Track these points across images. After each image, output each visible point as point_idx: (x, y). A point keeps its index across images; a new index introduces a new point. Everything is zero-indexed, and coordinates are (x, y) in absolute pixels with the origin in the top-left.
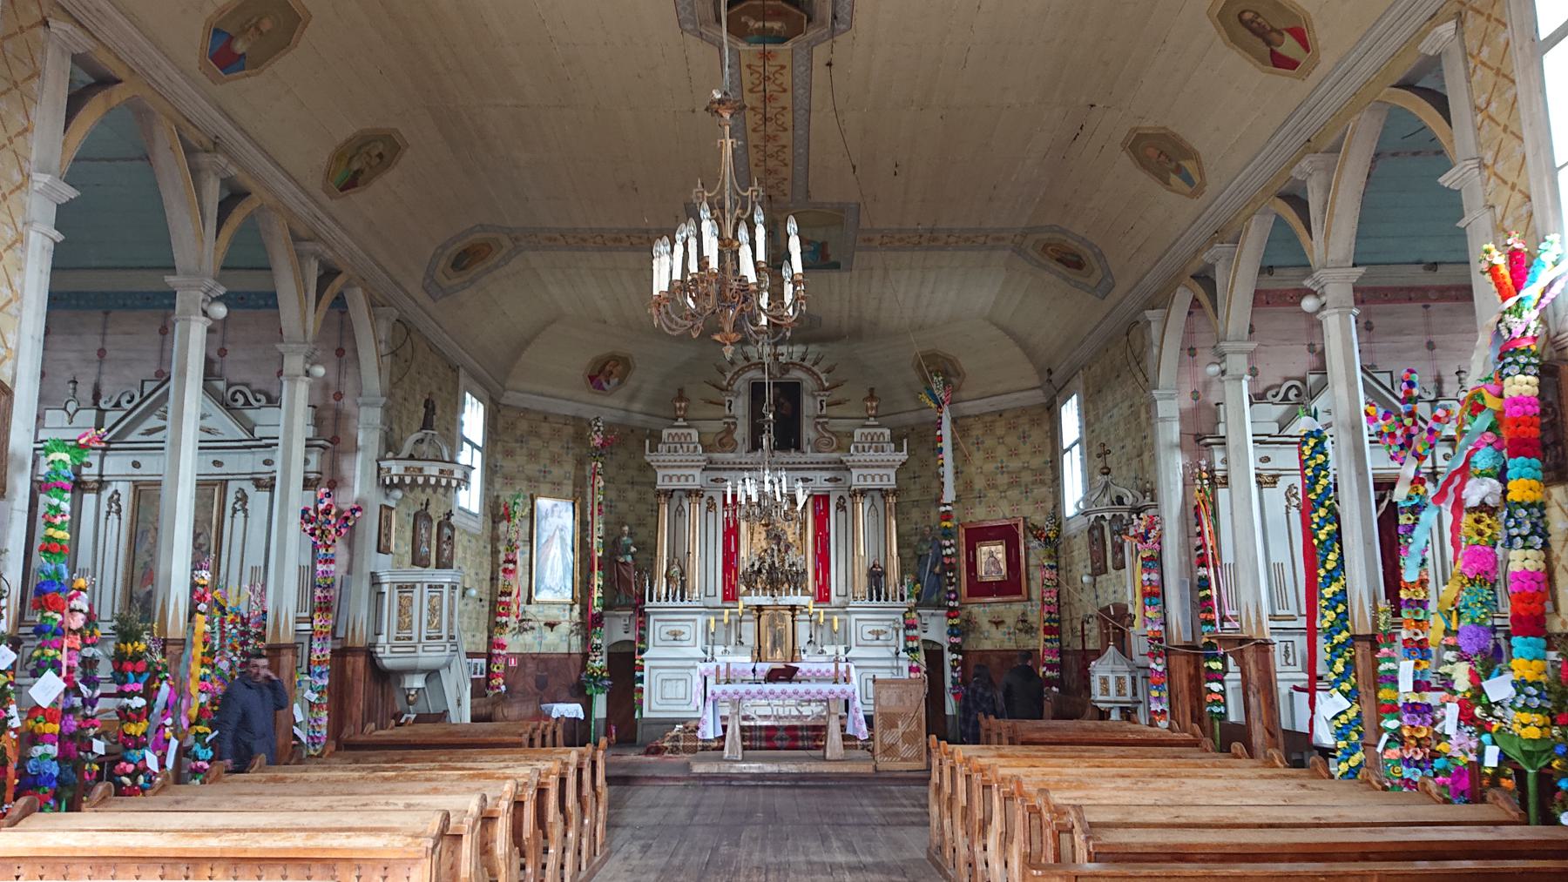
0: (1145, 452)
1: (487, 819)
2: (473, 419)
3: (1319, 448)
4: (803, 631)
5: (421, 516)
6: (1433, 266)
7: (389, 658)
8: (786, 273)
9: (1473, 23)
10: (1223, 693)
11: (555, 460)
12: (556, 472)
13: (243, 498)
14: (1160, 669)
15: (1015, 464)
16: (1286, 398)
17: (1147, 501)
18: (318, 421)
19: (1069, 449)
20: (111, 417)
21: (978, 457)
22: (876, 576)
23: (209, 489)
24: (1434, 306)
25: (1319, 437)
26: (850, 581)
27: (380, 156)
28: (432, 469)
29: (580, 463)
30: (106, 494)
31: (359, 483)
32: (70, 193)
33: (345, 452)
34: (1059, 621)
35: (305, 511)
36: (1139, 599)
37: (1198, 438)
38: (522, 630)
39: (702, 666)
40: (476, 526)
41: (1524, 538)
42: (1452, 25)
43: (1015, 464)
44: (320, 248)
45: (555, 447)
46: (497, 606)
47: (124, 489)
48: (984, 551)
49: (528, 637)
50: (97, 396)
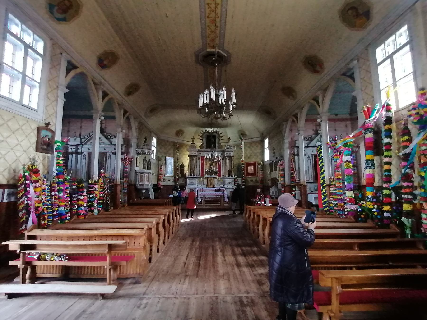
0: (281, 149)
1: (158, 224)
2: (154, 141)
3: (320, 148)
4: (216, 182)
5: (144, 160)
7: (138, 186)
8: (230, 103)
9: (362, 61)
10: (295, 194)
11: (169, 150)
13: (110, 156)
15: (255, 151)
16: (308, 140)
17: (282, 159)
18: (124, 141)
20: (83, 140)
22: (230, 172)
23: (102, 155)
25: (321, 146)
28: (146, 151)
29: (174, 150)
30: (83, 155)
31: (132, 151)
32: (67, 91)
33: (129, 147)
35: (122, 159)
37: (292, 147)
38: (164, 181)
39: (197, 188)
40: (155, 162)
41: (370, 167)
42: (356, 61)
43: (255, 151)
46: (159, 176)
47: (87, 154)
48: (249, 167)
49: (165, 182)
50: (80, 136)
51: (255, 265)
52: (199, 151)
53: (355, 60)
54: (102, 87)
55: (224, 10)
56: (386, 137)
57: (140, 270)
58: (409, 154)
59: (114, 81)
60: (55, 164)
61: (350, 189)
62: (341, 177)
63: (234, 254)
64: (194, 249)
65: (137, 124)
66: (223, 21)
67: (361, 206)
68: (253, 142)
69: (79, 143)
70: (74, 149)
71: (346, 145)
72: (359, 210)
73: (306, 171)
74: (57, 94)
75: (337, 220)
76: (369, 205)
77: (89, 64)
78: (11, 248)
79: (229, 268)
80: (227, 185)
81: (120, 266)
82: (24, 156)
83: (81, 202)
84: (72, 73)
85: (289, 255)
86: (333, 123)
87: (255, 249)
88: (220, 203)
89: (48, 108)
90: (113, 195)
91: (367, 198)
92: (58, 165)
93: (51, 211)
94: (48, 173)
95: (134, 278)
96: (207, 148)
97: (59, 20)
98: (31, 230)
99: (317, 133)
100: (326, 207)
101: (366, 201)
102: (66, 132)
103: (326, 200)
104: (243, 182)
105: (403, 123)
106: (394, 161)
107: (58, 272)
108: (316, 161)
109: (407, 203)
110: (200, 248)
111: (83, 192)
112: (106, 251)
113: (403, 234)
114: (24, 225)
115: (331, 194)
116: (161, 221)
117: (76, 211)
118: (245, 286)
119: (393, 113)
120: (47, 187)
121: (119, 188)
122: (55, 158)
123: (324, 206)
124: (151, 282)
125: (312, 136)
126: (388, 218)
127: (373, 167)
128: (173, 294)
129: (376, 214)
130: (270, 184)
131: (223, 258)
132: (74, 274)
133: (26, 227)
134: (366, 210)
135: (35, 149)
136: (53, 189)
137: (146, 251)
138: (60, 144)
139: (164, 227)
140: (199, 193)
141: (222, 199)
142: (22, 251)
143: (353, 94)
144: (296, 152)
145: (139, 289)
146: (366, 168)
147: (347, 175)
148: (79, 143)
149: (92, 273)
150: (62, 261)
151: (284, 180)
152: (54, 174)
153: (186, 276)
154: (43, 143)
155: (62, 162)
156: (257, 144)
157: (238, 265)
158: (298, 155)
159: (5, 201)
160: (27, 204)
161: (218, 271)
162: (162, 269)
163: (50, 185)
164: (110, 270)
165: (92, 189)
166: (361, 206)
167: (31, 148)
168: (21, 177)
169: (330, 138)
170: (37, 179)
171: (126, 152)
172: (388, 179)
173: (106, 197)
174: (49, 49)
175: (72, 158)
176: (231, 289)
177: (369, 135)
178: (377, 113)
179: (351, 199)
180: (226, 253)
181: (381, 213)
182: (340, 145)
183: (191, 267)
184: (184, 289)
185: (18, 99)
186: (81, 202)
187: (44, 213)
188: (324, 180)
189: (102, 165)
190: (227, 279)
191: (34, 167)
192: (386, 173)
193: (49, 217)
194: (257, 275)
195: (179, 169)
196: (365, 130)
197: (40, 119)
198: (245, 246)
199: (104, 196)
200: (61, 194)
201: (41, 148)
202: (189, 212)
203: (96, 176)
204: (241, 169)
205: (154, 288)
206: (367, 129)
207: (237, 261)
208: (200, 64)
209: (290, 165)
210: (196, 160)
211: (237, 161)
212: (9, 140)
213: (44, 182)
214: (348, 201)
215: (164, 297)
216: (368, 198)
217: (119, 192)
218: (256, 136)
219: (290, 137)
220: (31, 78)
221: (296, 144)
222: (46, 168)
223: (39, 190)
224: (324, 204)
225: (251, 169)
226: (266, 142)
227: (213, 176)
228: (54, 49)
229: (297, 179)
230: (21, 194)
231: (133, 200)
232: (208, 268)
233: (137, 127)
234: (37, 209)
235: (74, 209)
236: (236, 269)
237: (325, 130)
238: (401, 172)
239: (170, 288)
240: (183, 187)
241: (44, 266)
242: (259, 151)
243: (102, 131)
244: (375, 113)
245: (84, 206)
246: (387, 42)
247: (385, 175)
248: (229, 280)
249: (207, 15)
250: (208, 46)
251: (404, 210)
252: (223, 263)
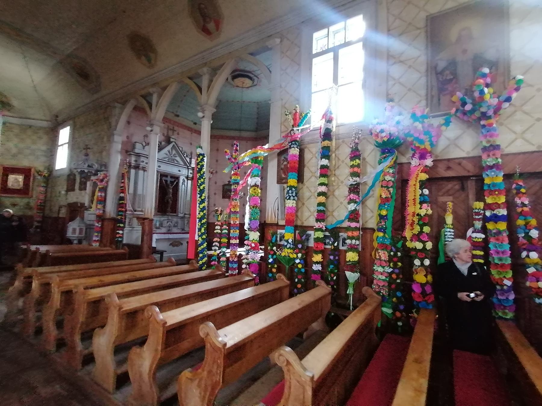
0: (104, 151)
3: (202, 160)
10: (123, 234)
14: (100, 226)
15: (34, 147)
17: (103, 168)
19: (62, 145)
24: (194, 134)
34: (44, 206)
37: (127, 152)
75: (144, 265)
151: (104, 207)
226: (65, 134)
242: (44, 148)
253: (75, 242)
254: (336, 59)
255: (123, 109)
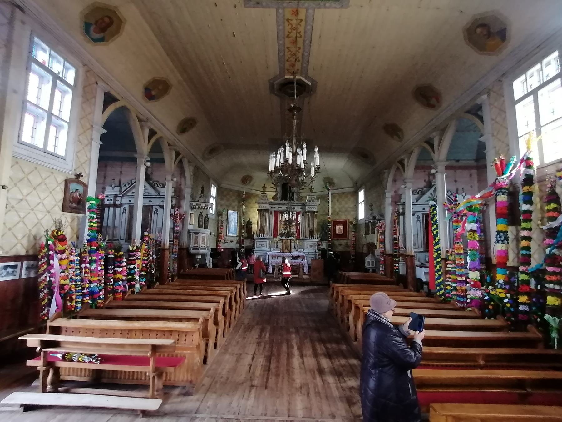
0: (381, 205)
2: (214, 190)
4: (293, 245)
5: (200, 215)
6: (458, 161)
7: (192, 250)
10: (398, 266)
11: (233, 201)
12: (234, 204)
13: (156, 210)
15: (347, 206)
16: (418, 193)
17: (382, 218)
18: (175, 192)
20: (123, 189)
21: (337, 204)
22: (311, 233)
23: (147, 209)
25: (435, 206)
26: (305, 233)
27: (191, 124)
28: (203, 204)
29: (239, 202)
30: (122, 208)
31: (185, 204)
32: (105, 131)
35: (171, 214)
36: (378, 243)
37: (396, 203)
38: (224, 242)
39: (268, 253)
40: (214, 217)
41: (502, 241)
43: (347, 206)
44: (176, 148)
45: (233, 198)
46: (218, 236)
48: (338, 227)
49: (226, 244)
51: (344, 374)
52: (271, 204)
53: (485, 94)
54: (149, 124)
55: (309, 27)
56: (526, 202)
57: (191, 375)
58: (557, 229)
59: (163, 116)
60: (87, 228)
61: (474, 269)
62: (462, 251)
63: (316, 355)
64: (263, 344)
65: (192, 168)
66: (307, 42)
67: (489, 294)
68: (343, 193)
69: (118, 193)
70: (111, 200)
71: (470, 208)
72: (486, 298)
73: (414, 236)
74: (92, 135)
76: (500, 293)
77: (132, 96)
78: (29, 345)
79: (309, 377)
80: (308, 250)
81: (167, 374)
82: (48, 217)
83: (118, 276)
84: (111, 108)
85: (388, 381)
86: (452, 172)
87: (344, 347)
88: (298, 274)
89: (79, 155)
90: (160, 262)
91: (497, 284)
92: (91, 228)
93: (81, 288)
94: (78, 238)
95: (184, 387)
96: (282, 200)
97: (95, 41)
98: (55, 318)
99: (430, 185)
100: (441, 289)
101: (496, 287)
102: (101, 187)
103: (441, 280)
104: (329, 246)
105: (549, 185)
106: (535, 235)
107: (87, 375)
108: (428, 221)
109: (553, 296)
110: (271, 342)
111: (121, 262)
112: (149, 354)
113: (547, 341)
114: (46, 309)
115: (447, 272)
116: (221, 306)
117: (112, 287)
118: (330, 406)
119: (535, 170)
120: (75, 258)
121: (167, 253)
122: (88, 219)
123: (438, 288)
124: (206, 393)
125: (423, 189)
126: (524, 312)
127: (506, 242)
128: (234, 414)
129: (508, 305)
130: (365, 250)
131: (301, 360)
132: (109, 378)
133: (49, 310)
134: (495, 300)
135: (61, 208)
136: (84, 259)
137: (200, 352)
138: (94, 202)
139: (224, 314)
140: (271, 260)
141: (301, 270)
142: (43, 350)
143: (482, 139)
144: (401, 210)
145: (190, 403)
146: (498, 241)
147: (470, 250)
148: (118, 193)
149: (131, 378)
150: (93, 363)
151: (385, 246)
152: (86, 241)
153: (252, 386)
154: (71, 200)
155: (95, 225)
156: (349, 196)
157: (321, 372)
158: (404, 214)
159: (23, 276)
160: (50, 281)
161: (293, 380)
162: (220, 374)
163: (80, 255)
164: (154, 377)
165: (133, 258)
166: (489, 294)
167: (57, 206)
168: (42, 247)
169: (448, 192)
170: (63, 248)
171: (176, 206)
172: (526, 260)
173: (151, 265)
174: (81, 80)
175: (109, 212)
176: (311, 410)
177: (502, 198)
178: (514, 168)
179: (475, 283)
180: (304, 352)
181: (515, 304)
182: (462, 208)
183: (258, 372)
184: (248, 407)
185: (41, 146)
186: (118, 276)
187: (71, 292)
188: (439, 252)
189: (145, 226)
190: (306, 393)
191: (59, 233)
192: (524, 252)
193: (78, 297)
194: (346, 390)
195: (245, 227)
196: (496, 190)
197: (70, 171)
198: (330, 341)
199: (148, 263)
200: (94, 266)
201: (70, 207)
202: (257, 287)
203: (138, 241)
204: (327, 228)
205: (210, 403)
206: (499, 189)
207: (319, 364)
208: (276, 95)
209: (392, 227)
210: (267, 215)
211: (322, 217)
212: (28, 198)
213: (72, 252)
214: (472, 285)
215: (222, 418)
216: (499, 283)
217: (167, 259)
218: (348, 187)
219: (394, 190)
220: (58, 117)
221: (401, 199)
222: (76, 231)
223: (65, 262)
224: (439, 286)
225: (340, 228)
227: (290, 238)
228: (87, 76)
229: (401, 246)
230: (42, 269)
231: (185, 271)
232: (281, 375)
233: (192, 174)
234: (62, 287)
235: (110, 285)
236: (318, 378)
237: (442, 182)
238: (545, 251)
239: (231, 403)
240: (249, 251)
241: (70, 368)
242: (352, 206)
243: (148, 178)
244: (510, 169)
245: (123, 281)
246: (529, 73)
247: (522, 254)
248: (308, 395)
249: (287, 33)
250: (286, 71)
251: (549, 305)
252: (301, 368)
253: (370, 271)
254: (536, 101)
255: (389, 173)
